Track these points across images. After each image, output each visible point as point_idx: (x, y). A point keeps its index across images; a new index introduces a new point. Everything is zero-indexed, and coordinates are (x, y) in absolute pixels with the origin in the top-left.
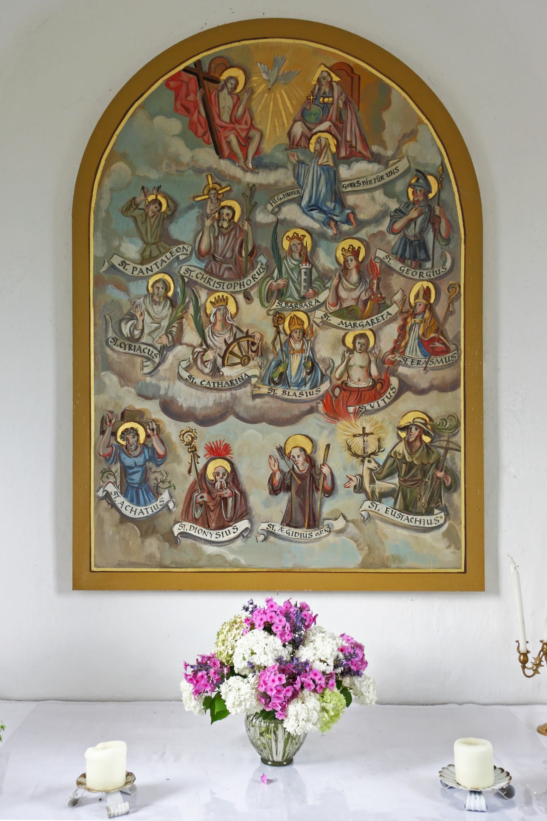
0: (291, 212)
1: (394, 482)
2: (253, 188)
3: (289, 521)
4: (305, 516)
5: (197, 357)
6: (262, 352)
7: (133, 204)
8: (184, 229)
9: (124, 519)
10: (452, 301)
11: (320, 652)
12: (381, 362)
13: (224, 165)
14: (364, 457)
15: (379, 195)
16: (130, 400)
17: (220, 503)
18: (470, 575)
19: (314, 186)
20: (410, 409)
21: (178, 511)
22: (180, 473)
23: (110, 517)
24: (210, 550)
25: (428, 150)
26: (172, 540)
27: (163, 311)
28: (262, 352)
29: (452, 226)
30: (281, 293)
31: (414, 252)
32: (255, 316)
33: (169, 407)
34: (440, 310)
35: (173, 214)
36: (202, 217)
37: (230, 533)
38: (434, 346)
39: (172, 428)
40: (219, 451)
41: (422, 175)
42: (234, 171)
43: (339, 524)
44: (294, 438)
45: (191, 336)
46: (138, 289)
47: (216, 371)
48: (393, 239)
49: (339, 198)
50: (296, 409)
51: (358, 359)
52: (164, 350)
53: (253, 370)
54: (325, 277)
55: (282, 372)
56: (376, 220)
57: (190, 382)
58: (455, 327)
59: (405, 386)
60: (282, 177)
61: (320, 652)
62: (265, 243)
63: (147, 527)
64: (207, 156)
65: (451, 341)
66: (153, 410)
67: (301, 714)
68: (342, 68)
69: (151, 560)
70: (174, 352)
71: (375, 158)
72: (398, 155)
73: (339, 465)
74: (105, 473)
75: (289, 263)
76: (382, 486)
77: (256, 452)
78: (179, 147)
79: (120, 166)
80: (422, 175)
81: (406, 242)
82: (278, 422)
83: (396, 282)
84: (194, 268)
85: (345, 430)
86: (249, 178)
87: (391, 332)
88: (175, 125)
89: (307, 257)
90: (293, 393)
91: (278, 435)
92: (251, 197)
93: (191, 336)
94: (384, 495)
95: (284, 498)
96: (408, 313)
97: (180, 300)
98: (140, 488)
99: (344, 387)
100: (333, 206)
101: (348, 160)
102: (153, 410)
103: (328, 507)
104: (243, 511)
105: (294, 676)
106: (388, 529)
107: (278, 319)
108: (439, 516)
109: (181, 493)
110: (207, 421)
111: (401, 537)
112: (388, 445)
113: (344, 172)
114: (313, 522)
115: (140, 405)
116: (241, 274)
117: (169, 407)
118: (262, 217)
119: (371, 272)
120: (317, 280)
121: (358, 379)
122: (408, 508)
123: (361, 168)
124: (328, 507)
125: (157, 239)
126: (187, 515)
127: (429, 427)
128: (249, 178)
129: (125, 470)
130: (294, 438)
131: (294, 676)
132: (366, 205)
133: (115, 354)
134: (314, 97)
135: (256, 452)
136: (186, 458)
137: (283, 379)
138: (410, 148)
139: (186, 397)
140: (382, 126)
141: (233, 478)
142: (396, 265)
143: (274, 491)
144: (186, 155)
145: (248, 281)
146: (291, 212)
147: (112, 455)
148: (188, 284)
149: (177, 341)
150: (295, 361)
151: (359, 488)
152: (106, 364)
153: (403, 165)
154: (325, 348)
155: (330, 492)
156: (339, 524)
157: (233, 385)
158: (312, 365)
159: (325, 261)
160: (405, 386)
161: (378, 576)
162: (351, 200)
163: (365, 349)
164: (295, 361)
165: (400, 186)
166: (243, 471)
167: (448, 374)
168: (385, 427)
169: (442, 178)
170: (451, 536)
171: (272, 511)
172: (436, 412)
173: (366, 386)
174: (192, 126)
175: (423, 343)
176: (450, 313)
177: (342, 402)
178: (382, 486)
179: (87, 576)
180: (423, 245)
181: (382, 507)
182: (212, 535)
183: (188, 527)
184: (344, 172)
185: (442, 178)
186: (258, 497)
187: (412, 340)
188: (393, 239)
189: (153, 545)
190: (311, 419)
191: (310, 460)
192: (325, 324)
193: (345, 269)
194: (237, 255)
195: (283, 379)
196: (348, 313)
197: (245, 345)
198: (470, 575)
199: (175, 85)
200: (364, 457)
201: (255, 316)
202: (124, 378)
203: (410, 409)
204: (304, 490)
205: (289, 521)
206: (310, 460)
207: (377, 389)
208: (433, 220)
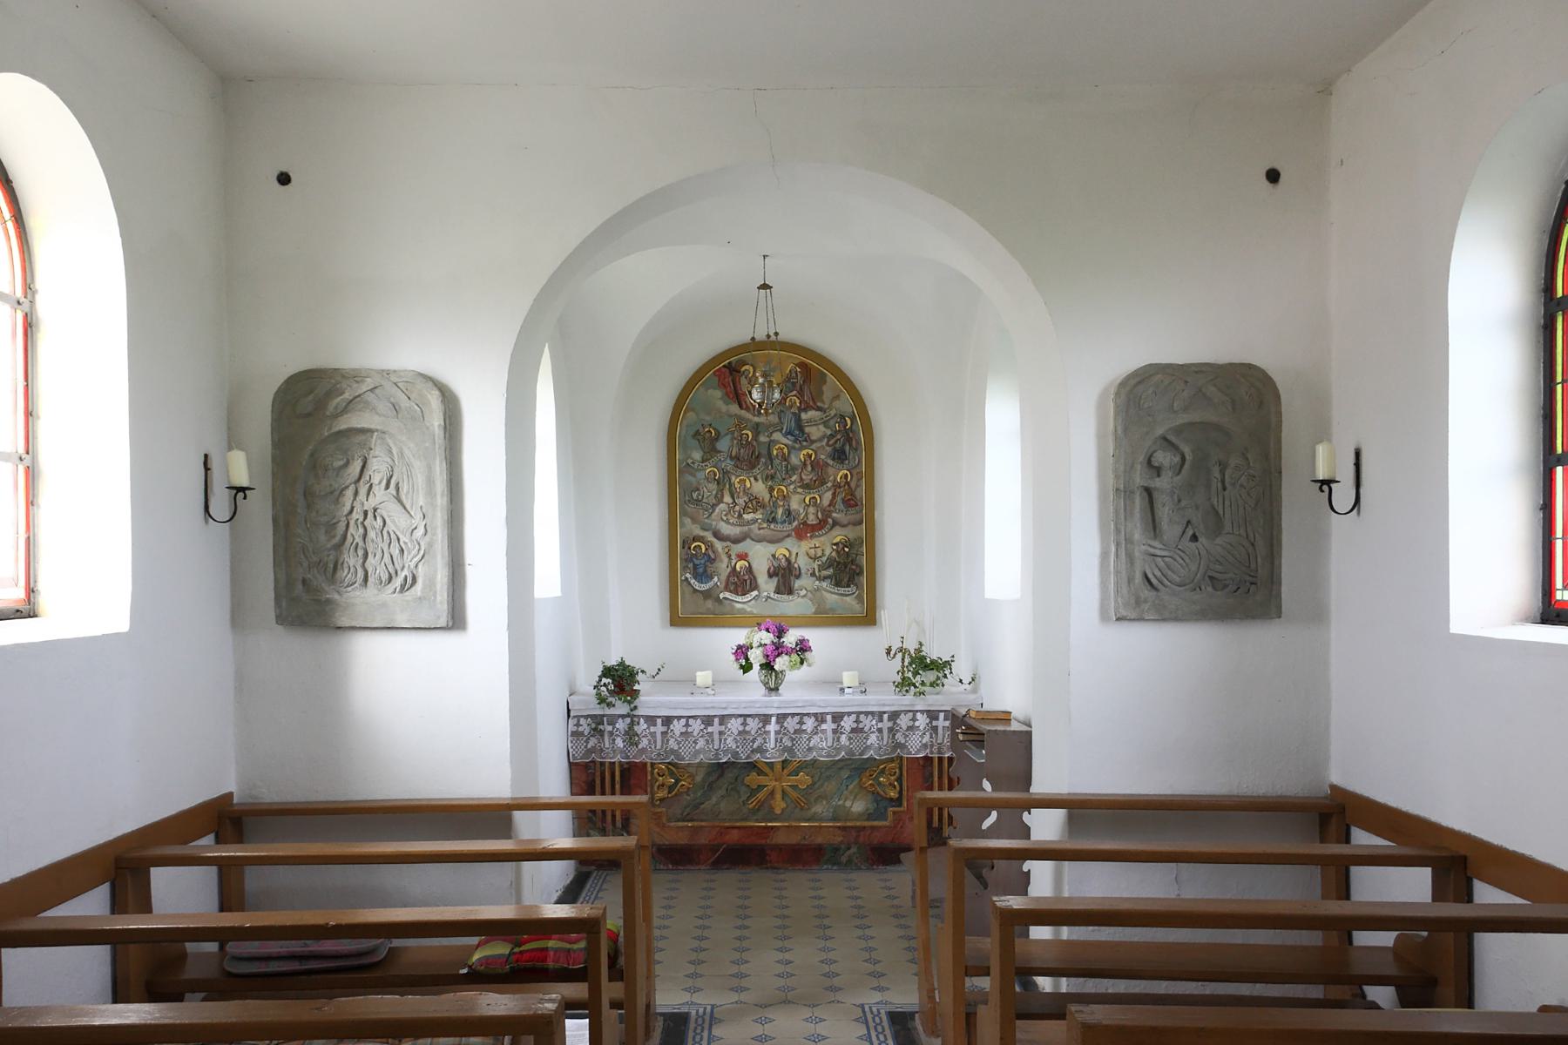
0: (777, 436)
1: (830, 572)
2: (758, 424)
3: (778, 591)
4: (785, 588)
5: (731, 508)
6: (763, 506)
7: (697, 433)
8: (724, 445)
9: (695, 591)
10: (860, 479)
11: (790, 639)
12: (823, 511)
13: (743, 413)
14: (815, 559)
15: (822, 427)
16: (698, 532)
17: (743, 582)
18: (868, 618)
19: (789, 422)
20: (838, 535)
21: (721, 585)
22: (723, 567)
23: (688, 590)
24: (738, 606)
25: (846, 404)
26: (718, 600)
27: (713, 486)
28: (763, 506)
29: (858, 442)
30: (772, 477)
31: (840, 456)
32: (759, 488)
33: (717, 535)
34: (853, 485)
35: (717, 438)
36: (733, 439)
37: (748, 597)
38: (851, 502)
39: (719, 545)
40: (743, 557)
41: (842, 417)
42: (748, 415)
43: (803, 592)
44: (781, 551)
45: (727, 499)
46: (700, 475)
47: (740, 516)
48: (829, 449)
49: (801, 429)
50: (781, 535)
51: (812, 510)
52: (714, 506)
53: (759, 516)
54: (794, 469)
55: (777, 519)
56: (820, 440)
57: (727, 522)
58: (861, 493)
59: (835, 523)
60: (773, 419)
61: (790, 639)
62: (764, 452)
63: (707, 595)
64: (734, 409)
65: (857, 502)
66: (709, 536)
67: (781, 663)
68: (802, 365)
69: (709, 612)
70: (439, 514)
71: (819, 409)
72: (830, 408)
73: (802, 562)
74: (684, 568)
75: (776, 462)
76: (825, 573)
77: (761, 557)
78: (720, 404)
79: (691, 415)
80: (842, 417)
81: (835, 450)
82: (771, 542)
83: (831, 471)
84: (729, 464)
85: (805, 546)
86: (756, 419)
87: (828, 495)
88: (718, 393)
89: (785, 459)
90: (779, 527)
91: (771, 548)
92: (757, 429)
93: (727, 499)
94: (825, 578)
95: (775, 580)
96: (837, 486)
97: (722, 481)
98: (703, 576)
99: (805, 523)
100: (798, 432)
101: (805, 410)
102: (709, 536)
103: (797, 584)
104: (755, 587)
105: (779, 649)
106: (828, 595)
107: (771, 490)
108: (853, 589)
109: (724, 577)
110: (736, 541)
111: (833, 597)
112: (827, 553)
113: (804, 416)
114: (790, 592)
115: (702, 533)
116: (753, 467)
117: (717, 535)
118: (763, 439)
119: (816, 465)
120: (791, 470)
121: (812, 520)
122: (838, 584)
123: (812, 414)
124: (797, 584)
125: (711, 450)
126: (726, 589)
127: (848, 543)
128: (756, 419)
129: (695, 566)
130: (781, 551)
131: (779, 649)
132: (815, 432)
133: (690, 508)
134: (789, 378)
135: (761, 557)
136: (726, 560)
137: (774, 520)
138: (837, 404)
139: (726, 529)
140: (822, 393)
141: (750, 569)
142: (830, 462)
143: (770, 576)
144: (724, 408)
145: (756, 471)
146: (777, 436)
147: (688, 559)
148: (726, 473)
149: (721, 501)
150: (780, 511)
151: (813, 574)
152: (684, 513)
153: (833, 412)
154: (795, 504)
155: (798, 577)
156: (803, 592)
157: (748, 523)
158: (788, 513)
159: (794, 460)
160: (835, 523)
161: (826, 618)
162: (807, 430)
163: (815, 504)
164: (780, 511)
165: (832, 423)
166: (754, 566)
167: (857, 517)
168: (826, 544)
169: (853, 419)
170: (859, 599)
171: (767, 585)
172: (851, 536)
173: (991, 591)
174: (727, 394)
175: (844, 501)
176: (857, 486)
177: (804, 531)
178: (825, 573)
179: (677, 620)
180: (844, 452)
181: (824, 584)
182: (739, 599)
183: (727, 595)
184: (804, 416)
185: (853, 419)
186: (762, 578)
187: (839, 499)
188: (829, 449)
189: (709, 604)
190: (789, 540)
191: (788, 560)
192: (795, 492)
193: (805, 464)
194: (750, 458)
195: (774, 520)
196: (806, 487)
197: (755, 503)
198: (868, 618)
199: (718, 374)
200: (815, 559)
201: (759, 488)
202: (694, 521)
203: (838, 535)
204: (785, 576)
205: (778, 591)
206: (788, 560)
207: (821, 525)
208: (849, 440)
